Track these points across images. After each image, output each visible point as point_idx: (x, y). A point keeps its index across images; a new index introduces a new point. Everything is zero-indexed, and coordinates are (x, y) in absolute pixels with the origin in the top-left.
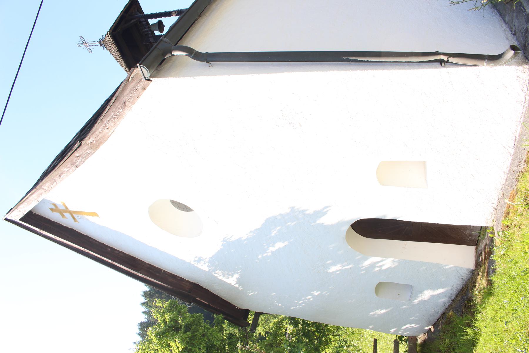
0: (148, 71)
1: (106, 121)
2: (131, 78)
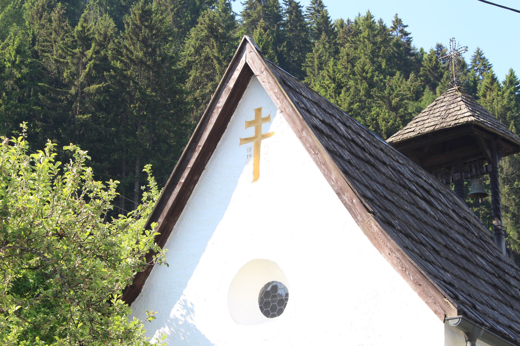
0: (455, 324)
2: (448, 301)
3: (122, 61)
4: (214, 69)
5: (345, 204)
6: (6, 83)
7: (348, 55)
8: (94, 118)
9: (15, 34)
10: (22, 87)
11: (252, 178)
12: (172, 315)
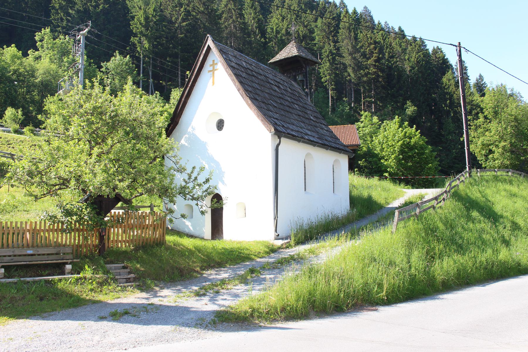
3: (195, 12)
4: (232, 13)
5: (240, 94)
6: (151, 23)
7: (288, 4)
8: (186, 36)
9: (153, 3)
10: (157, 25)
11: (212, 84)
12: (188, 131)
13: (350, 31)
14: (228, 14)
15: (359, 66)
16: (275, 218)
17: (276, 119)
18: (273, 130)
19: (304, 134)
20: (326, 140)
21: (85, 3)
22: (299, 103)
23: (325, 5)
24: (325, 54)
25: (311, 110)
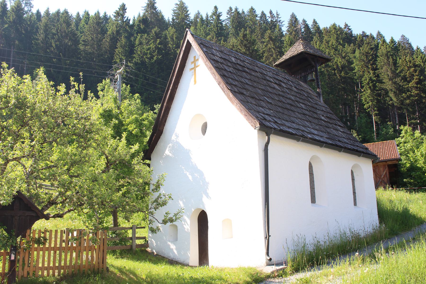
1: (239, 105)
4: (273, 52)
5: (221, 88)
7: (326, 40)
13: (388, 58)
14: (269, 53)
15: (400, 90)
16: (266, 238)
17: (267, 114)
18: (258, 125)
19: (307, 132)
20: (339, 141)
21: (142, 57)
22: (306, 102)
23: (362, 38)
24: (366, 82)
25: (323, 111)
